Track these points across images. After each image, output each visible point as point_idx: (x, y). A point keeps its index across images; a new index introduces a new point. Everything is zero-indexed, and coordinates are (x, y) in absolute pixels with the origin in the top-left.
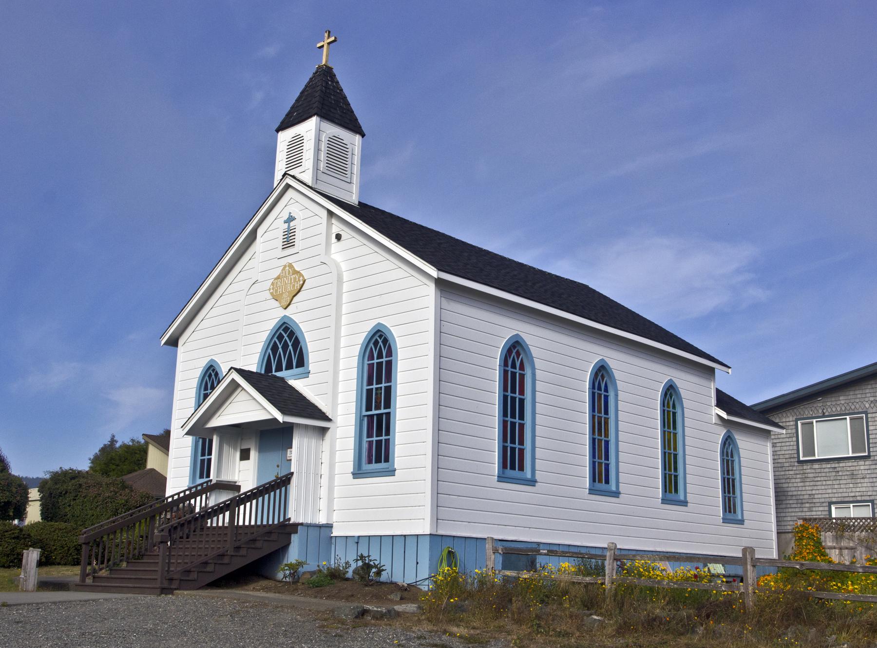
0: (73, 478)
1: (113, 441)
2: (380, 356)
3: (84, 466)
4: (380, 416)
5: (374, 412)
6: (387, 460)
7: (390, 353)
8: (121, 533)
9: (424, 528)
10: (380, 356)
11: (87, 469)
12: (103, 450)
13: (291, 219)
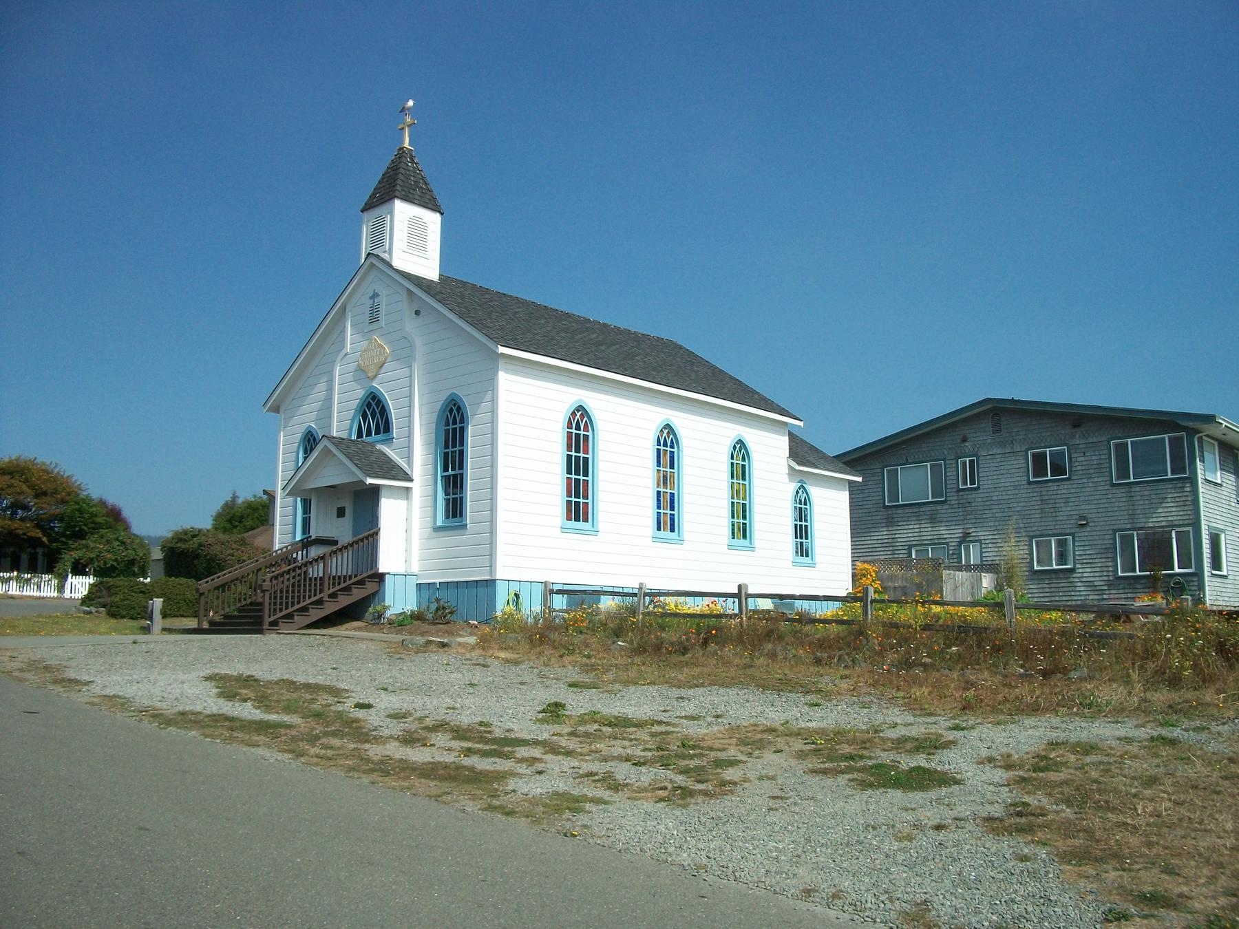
0: (194, 536)
1: (235, 497)
2: (455, 423)
3: (206, 523)
4: (455, 476)
5: (450, 472)
6: (461, 516)
7: (462, 421)
8: (904, 698)
9: (500, 574)
10: (455, 423)
11: (209, 527)
12: (226, 505)
13: (375, 295)
